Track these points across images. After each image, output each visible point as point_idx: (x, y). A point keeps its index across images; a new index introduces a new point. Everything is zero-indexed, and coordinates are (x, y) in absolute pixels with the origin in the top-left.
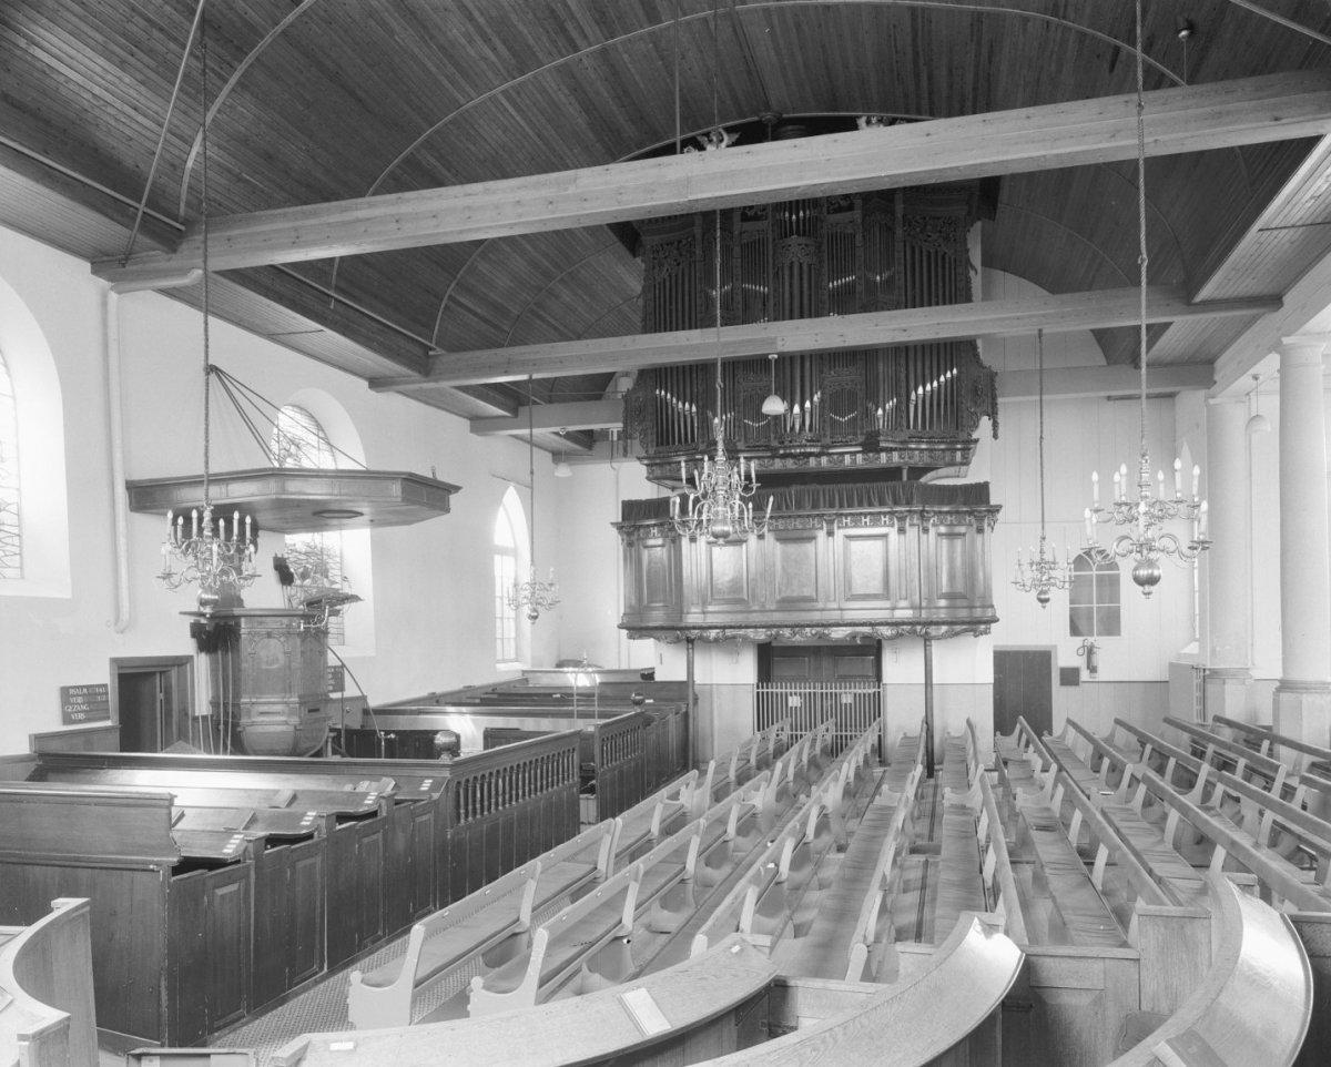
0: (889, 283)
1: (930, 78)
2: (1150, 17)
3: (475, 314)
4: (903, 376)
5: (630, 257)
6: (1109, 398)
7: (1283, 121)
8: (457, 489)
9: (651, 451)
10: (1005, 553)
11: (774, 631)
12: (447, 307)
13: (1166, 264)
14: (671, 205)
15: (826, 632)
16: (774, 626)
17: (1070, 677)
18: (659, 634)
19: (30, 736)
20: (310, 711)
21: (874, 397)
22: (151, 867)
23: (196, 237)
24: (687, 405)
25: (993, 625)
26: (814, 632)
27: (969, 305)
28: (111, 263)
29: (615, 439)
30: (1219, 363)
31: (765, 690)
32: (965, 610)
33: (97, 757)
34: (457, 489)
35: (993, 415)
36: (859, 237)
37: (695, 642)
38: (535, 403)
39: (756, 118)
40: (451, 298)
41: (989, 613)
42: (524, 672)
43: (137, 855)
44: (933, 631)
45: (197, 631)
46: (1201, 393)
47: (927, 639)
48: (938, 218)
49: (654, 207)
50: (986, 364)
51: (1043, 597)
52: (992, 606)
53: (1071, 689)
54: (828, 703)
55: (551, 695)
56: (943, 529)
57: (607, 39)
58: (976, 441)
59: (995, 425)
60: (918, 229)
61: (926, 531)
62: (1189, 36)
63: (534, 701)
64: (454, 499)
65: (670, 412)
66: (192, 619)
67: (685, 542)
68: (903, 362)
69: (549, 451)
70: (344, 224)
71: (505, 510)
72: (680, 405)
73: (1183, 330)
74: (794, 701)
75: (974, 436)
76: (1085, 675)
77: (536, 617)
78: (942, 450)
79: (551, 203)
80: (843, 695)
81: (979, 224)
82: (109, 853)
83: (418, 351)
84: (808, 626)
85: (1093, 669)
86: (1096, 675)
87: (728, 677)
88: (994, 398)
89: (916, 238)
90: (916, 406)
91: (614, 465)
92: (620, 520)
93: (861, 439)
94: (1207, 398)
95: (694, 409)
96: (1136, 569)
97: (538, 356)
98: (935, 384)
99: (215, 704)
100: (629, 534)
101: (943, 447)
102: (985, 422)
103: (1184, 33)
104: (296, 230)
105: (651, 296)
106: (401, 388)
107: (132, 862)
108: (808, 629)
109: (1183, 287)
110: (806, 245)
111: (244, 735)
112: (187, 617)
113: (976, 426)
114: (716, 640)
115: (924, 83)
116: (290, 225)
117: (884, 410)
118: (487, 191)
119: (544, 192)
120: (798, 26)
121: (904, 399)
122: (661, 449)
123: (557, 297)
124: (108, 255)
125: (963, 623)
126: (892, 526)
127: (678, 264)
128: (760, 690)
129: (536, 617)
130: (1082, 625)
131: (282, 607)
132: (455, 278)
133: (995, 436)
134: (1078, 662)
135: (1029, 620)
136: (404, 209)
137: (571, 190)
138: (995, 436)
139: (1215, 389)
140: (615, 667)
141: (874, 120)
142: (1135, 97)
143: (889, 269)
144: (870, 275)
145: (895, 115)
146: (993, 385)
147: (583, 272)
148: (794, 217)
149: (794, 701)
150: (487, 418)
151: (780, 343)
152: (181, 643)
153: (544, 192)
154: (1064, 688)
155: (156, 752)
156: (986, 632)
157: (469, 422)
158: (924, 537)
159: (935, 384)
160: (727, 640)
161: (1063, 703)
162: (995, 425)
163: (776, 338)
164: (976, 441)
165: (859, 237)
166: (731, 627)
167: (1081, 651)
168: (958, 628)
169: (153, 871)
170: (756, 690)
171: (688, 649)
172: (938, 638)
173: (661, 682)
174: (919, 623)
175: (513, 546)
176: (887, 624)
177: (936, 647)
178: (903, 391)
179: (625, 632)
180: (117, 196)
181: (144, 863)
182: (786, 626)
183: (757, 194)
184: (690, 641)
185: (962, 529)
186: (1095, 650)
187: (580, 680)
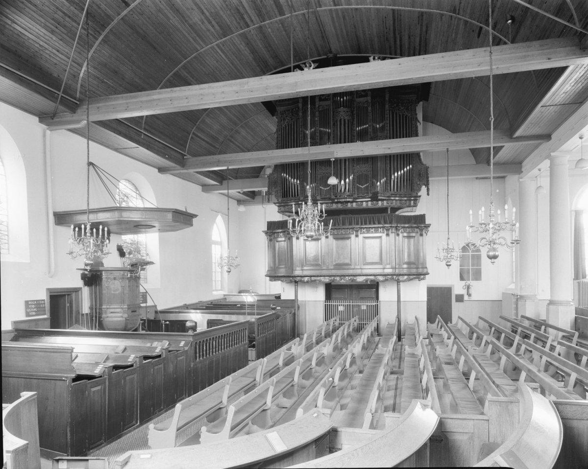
0: (383, 129)
3: (204, 140)
4: (388, 169)
6: (477, 178)
8: (196, 216)
9: (280, 200)
10: (432, 246)
11: (332, 278)
12: (192, 138)
15: (355, 278)
17: (460, 298)
18: (283, 279)
20: (132, 312)
21: (375, 177)
24: (295, 180)
28: (47, 118)
29: (264, 194)
30: (524, 164)
31: (328, 303)
34: (196, 216)
35: (427, 185)
36: (370, 108)
37: (299, 283)
38: (230, 179)
39: (325, 57)
40: (194, 133)
41: (425, 271)
42: (224, 295)
43: (57, 373)
44: (401, 278)
46: (517, 176)
51: (448, 264)
52: (426, 268)
53: (460, 304)
54: (355, 309)
55: (236, 305)
56: (405, 234)
58: (420, 196)
59: (428, 190)
60: (395, 105)
61: (398, 235)
65: (288, 183)
66: (82, 272)
67: (294, 239)
68: (388, 162)
71: (216, 224)
72: (292, 180)
73: (509, 149)
74: (341, 308)
75: (419, 194)
76: (466, 298)
77: (230, 272)
78: (405, 200)
80: (362, 306)
81: (421, 103)
84: (347, 276)
85: (469, 295)
86: (470, 297)
87: (312, 299)
88: (428, 178)
89: (395, 108)
90: (394, 181)
91: (264, 206)
92: (266, 230)
93: (370, 195)
95: (298, 182)
98: (402, 172)
100: (270, 236)
101: (406, 199)
102: (424, 188)
105: (280, 133)
106: (172, 172)
108: (347, 277)
113: (420, 190)
114: (307, 282)
117: (380, 183)
121: (389, 178)
122: (284, 199)
123: (239, 133)
125: (414, 275)
126: (384, 233)
127: (292, 119)
128: (326, 303)
129: (230, 272)
130: (465, 276)
131: (121, 267)
133: (428, 194)
134: (464, 292)
135: (442, 274)
138: (428, 194)
139: (521, 175)
140: (264, 294)
142: (489, 48)
143: (382, 122)
144: (374, 125)
146: (427, 172)
147: (250, 122)
148: (342, 99)
149: (341, 308)
150: (209, 185)
151: (335, 154)
154: (458, 303)
156: (423, 279)
158: (397, 237)
159: (402, 172)
160: (312, 282)
161: (457, 310)
162: (428, 190)
164: (420, 196)
165: (370, 108)
167: (464, 287)
168: (412, 277)
169: (64, 380)
170: (324, 303)
172: (403, 281)
174: (395, 275)
176: (381, 275)
178: (389, 174)
179: (268, 278)
184: (296, 282)
185: (414, 234)
186: (470, 287)
187: (249, 299)
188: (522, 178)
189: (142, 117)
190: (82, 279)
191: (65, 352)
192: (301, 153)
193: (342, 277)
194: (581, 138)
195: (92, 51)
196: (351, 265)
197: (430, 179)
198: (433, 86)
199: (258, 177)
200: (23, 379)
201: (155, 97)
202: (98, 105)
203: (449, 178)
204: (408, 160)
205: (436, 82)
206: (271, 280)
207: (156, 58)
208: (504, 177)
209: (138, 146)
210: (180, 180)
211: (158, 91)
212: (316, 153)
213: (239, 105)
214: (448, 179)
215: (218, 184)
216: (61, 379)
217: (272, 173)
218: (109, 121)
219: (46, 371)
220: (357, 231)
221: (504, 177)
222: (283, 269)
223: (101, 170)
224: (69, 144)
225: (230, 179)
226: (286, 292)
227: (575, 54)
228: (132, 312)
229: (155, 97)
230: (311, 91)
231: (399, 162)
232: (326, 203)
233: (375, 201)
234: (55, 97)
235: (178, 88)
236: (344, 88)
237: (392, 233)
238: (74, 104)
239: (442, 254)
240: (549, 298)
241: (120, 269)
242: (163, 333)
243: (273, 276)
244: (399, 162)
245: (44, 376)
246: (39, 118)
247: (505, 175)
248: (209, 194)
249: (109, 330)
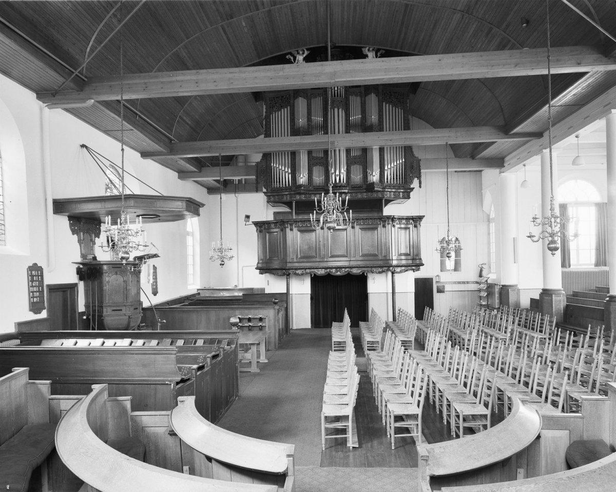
1: (406, 34)
2: (596, 18)
3: (188, 124)
5: (254, 101)
6: (456, 171)
7: (582, 65)
8: (203, 205)
13: (509, 116)
14: (327, 83)
16: (327, 268)
19: (15, 323)
20: (134, 309)
22: (167, 382)
23: (93, 85)
25: (421, 267)
26: (346, 270)
27: (409, 131)
28: (46, 94)
29: (237, 183)
30: (506, 159)
32: (410, 261)
33: (41, 333)
34: (203, 205)
35: (419, 177)
38: (209, 166)
42: (198, 290)
43: (158, 377)
45: (79, 272)
46: (498, 170)
47: (289, 275)
48: (396, 93)
49: (319, 83)
50: (417, 156)
51: (449, 255)
57: (272, 6)
58: (413, 188)
59: (420, 183)
62: (527, 26)
63: (233, 302)
64: (201, 210)
66: (77, 266)
67: (288, 230)
69: (205, 187)
70: (170, 82)
73: (502, 143)
75: (412, 186)
77: (223, 265)
79: (271, 79)
82: (144, 377)
83: (167, 140)
84: (344, 268)
88: (420, 170)
89: (405, 99)
91: (236, 195)
94: (500, 173)
96: (549, 244)
97: (225, 145)
99: (87, 306)
102: (416, 181)
103: (525, 25)
104: (145, 83)
106: (153, 157)
107: (156, 381)
108: (343, 269)
109: (506, 129)
110: (341, 101)
111: (105, 322)
112: (75, 264)
113: (412, 182)
115: (403, 35)
116: (143, 81)
118: (240, 72)
119: (269, 74)
120: (355, 7)
124: (47, 91)
129: (223, 265)
131: (110, 260)
132: (183, 107)
133: (420, 187)
136: (200, 77)
137: (281, 73)
138: (420, 187)
139: (503, 169)
141: (371, 49)
142: (546, 49)
145: (380, 47)
150: (187, 172)
152: (71, 277)
153: (269, 74)
155: (76, 330)
157: (177, 174)
158: (393, 229)
162: (420, 183)
163: (334, 141)
164: (413, 188)
166: (309, 269)
169: (167, 384)
171: (287, 278)
172: (397, 273)
173: (269, 294)
175: (192, 231)
177: (396, 275)
179: (258, 271)
180: (63, 63)
181: (163, 381)
182: (333, 268)
183: (365, 80)
188: (503, 172)
189: (138, 100)
190: (78, 274)
191: (169, 354)
192: (299, 142)
193: (338, 270)
194: (577, 137)
195: (102, 25)
196: (378, 256)
197: (422, 171)
198: (422, 86)
199: (228, 165)
200: (114, 385)
201: (179, 78)
202: (109, 84)
203: (449, 170)
204: (275, 157)
205: (426, 82)
206: (261, 273)
207: (157, 38)
208: (481, 171)
209: (133, 129)
210: (160, 166)
211: (152, 74)
212: (316, 143)
213: (230, 94)
214: (447, 172)
215: (197, 171)
216: (163, 383)
217: (261, 161)
218: (111, 101)
219: (145, 374)
220: (291, 225)
221: (481, 171)
222: (273, 262)
223: (94, 152)
224: (65, 126)
225: (209, 166)
226: (274, 285)
227: (601, 61)
228: (134, 309)
229: (179, 78)
230: (350, 81)
231: (392, 156)
232: (278, 195)
233: (370, 192)
234: (67, 71)
235: (205, 71)
236: (384, 80)
237: (295, 227)
238: (82, 81)
239: (216, 255)
240: (542, 287)
241: (108, 263)
242: (159, 331)
243: (264, 269)
244: (392, 156)
245: (141, 380)
246: (37, 94)
247: (481, 169)
248: (184, 182)
249: (109, 329)
